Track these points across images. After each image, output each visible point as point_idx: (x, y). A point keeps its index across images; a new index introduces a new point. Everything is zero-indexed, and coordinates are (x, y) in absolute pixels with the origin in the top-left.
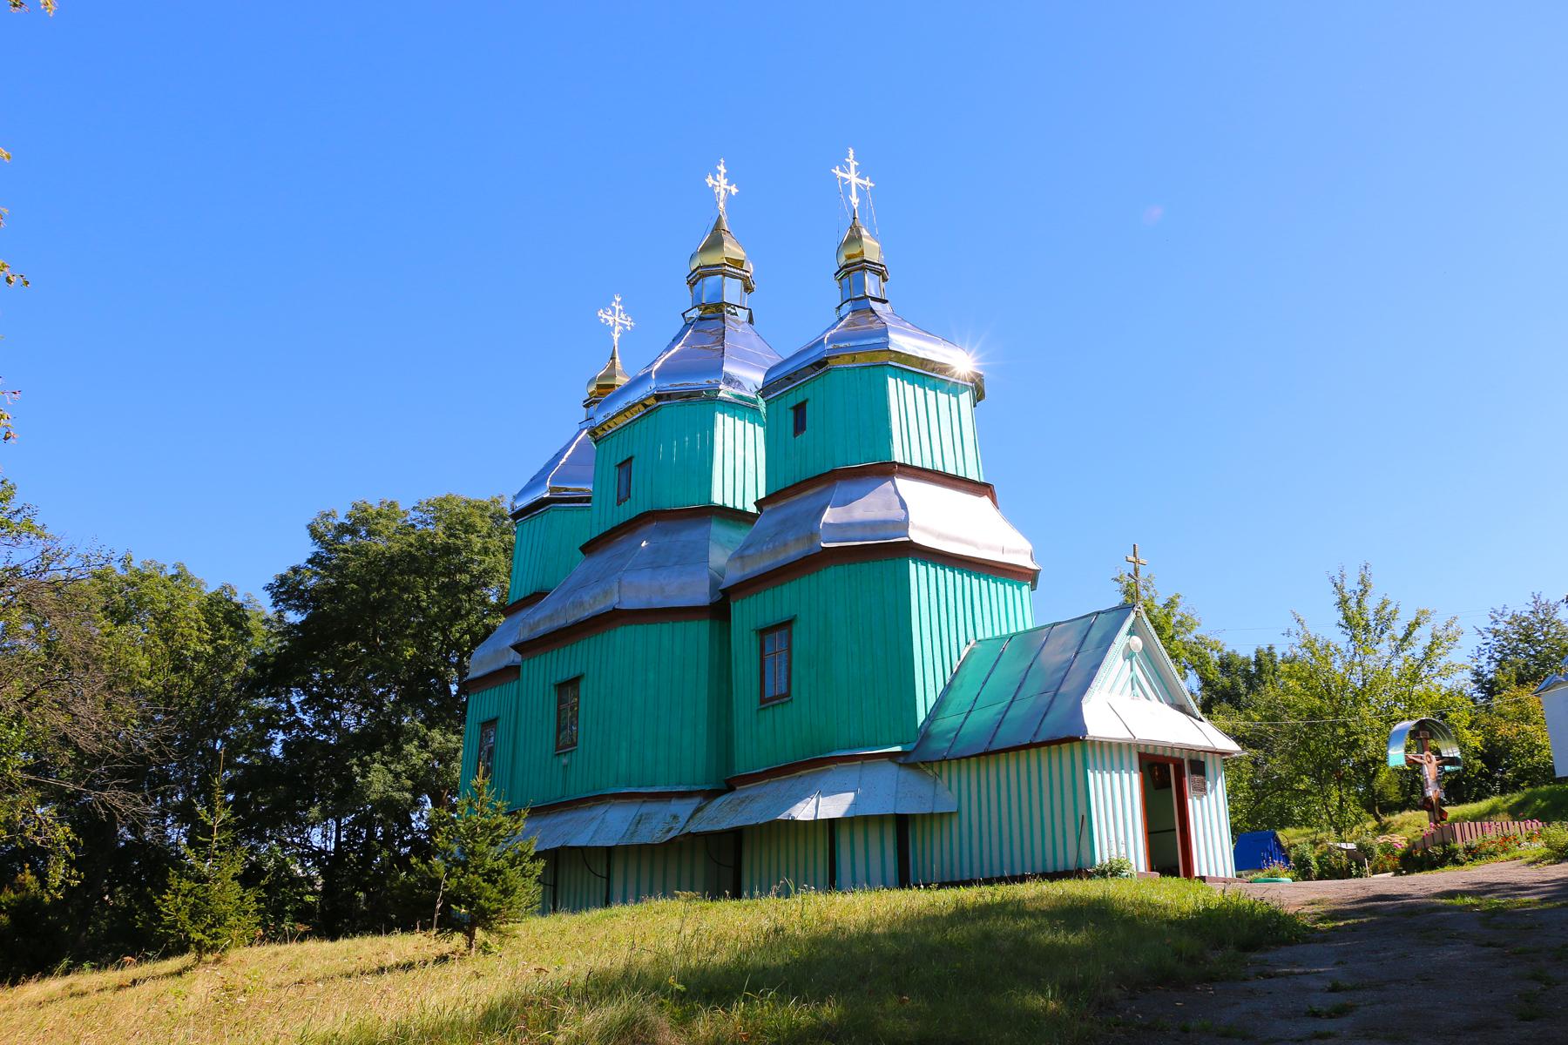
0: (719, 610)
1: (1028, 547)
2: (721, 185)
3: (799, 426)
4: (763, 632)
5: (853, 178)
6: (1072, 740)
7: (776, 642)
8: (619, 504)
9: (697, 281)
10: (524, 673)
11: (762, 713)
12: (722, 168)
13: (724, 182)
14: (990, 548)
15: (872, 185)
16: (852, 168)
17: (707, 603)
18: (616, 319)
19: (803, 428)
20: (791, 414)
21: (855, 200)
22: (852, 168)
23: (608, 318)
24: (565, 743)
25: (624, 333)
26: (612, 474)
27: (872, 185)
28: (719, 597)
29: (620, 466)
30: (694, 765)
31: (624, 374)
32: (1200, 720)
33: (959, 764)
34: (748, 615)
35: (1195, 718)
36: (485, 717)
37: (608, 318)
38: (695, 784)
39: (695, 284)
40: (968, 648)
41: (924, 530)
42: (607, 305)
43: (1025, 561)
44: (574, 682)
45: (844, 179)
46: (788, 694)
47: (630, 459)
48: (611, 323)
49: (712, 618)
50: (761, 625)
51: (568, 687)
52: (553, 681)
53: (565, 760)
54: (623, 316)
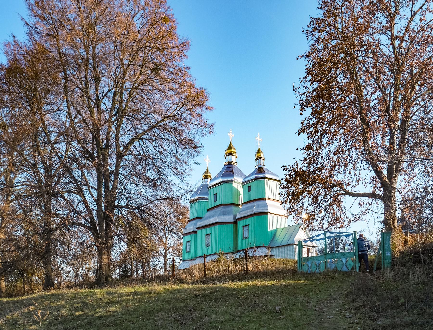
0: (235, 223)
2: (231, 135)
3: (249, 190)
4: (243, 226)
5: (259, 139)
6: (292, 244)
7: (245, 228)
8: (214, 202)
12: (231, 131)
13: (231, 136)
19: (250, 191)
20: (248, 188)
30: (231, 250)
34: (241, 224)
44: (250, 186)
46: (248, 237)
47: (216, 194)
49: (234, 224)
50: (243, 225)
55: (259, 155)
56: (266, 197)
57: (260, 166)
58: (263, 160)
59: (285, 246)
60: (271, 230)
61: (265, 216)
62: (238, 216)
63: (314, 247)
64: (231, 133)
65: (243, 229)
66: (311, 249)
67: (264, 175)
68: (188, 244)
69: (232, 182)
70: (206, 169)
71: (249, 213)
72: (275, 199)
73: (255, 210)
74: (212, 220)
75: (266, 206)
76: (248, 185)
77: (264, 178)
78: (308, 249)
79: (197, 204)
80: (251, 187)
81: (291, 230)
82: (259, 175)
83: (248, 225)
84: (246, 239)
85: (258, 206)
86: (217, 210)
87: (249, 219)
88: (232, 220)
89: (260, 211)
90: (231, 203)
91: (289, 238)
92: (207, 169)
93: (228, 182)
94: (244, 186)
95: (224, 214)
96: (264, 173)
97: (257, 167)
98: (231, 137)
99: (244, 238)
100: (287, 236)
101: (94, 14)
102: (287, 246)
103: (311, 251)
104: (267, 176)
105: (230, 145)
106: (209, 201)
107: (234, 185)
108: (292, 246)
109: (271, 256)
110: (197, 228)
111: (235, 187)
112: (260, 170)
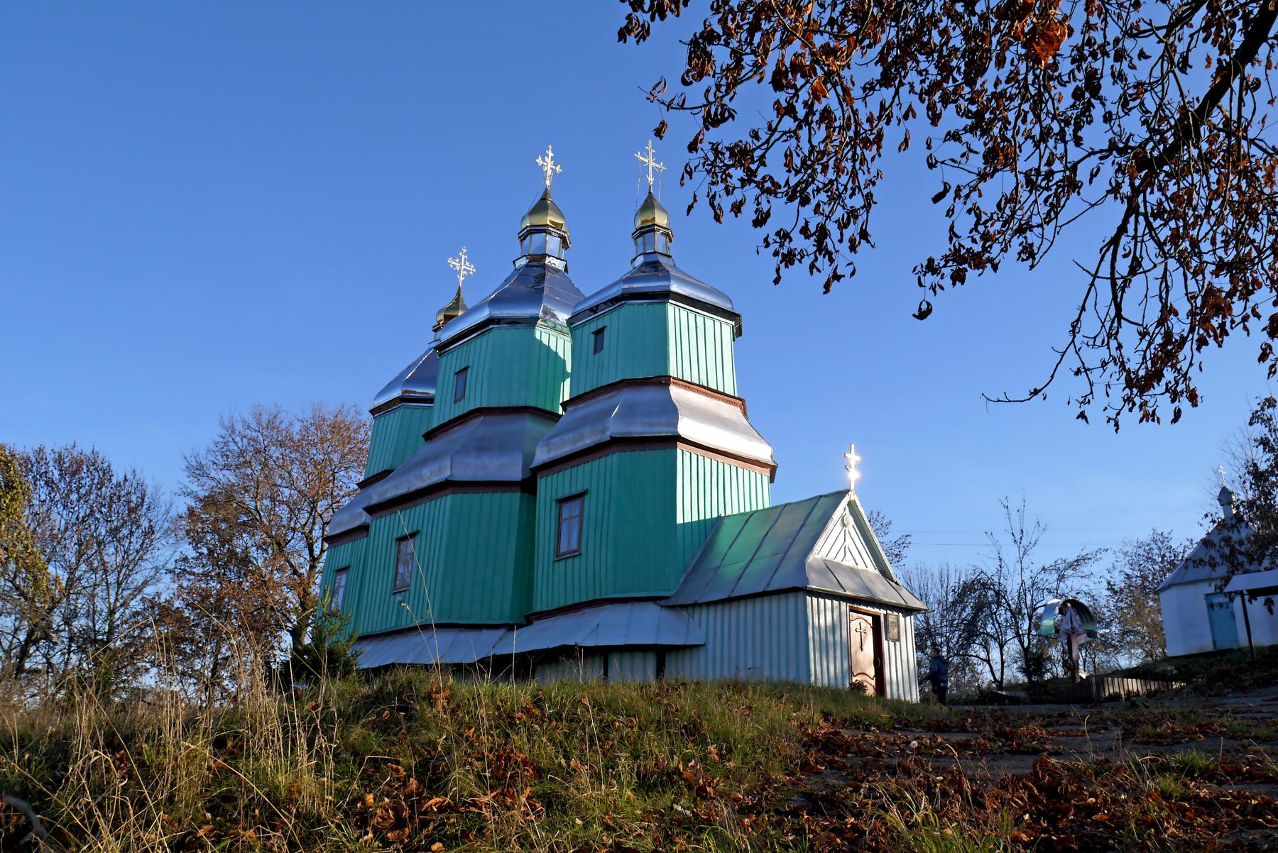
0: (528, 486)
2: (548, 164)
3: (598, 348)
4: (562, 501)
6: (795, 590)
8: (455, 402)
10: (372, 530)
11: (557, 564)
16: (650, 154)
18: (463, 267)
19: (602, 348)
20: (592, 337)
22: (650, 154)
25: (467, 277)
34: (549, 487)
47: (466, 369)
52: (395, 536)
55: (648, 216)
56: (673, 372)
57: (651, 258)
58: (663, 238)
59: (758, 601)
60: (688, 520)
61: (653, 456)
62: (541, 456)
63: (908, 611)
64: (548, 160)
66: (891, 619)
67: (665, 283)
68: (343, 579)
69: (532, 322)
70: (454, 295)
71: (588, 441)
72: (713, 386)
73: (615, 428)
74: (429, 476)
75: (671, 411)
76: (594, 327)
77: (666, 295)
78: (876, 618)
79: (393, 419)
80: (606, 332)
81: (786, 525)
82: (635, 286)
83: (582, 495)
84: (569, 561)
85: (630, 412)
86: (461, 434)
88: (516, 474)
89: (638, 429)
90: (522, 404)
91: (778, 557)
92: (459, 294)
93: (514, 322)
94: (578, 332)
95: (482, 447)
96: (667, 277)
97: (640, 260)
98: (549, 172)
99: (560, 557)
100: (767, 550)
102: (766, 599)
103: (893, 631)
104: (675, 288)
105: (544, 199)
107: (542, 334)
108: (791, 597)
110: (371, 510)
111: (553, 348)
112: (653, 266)
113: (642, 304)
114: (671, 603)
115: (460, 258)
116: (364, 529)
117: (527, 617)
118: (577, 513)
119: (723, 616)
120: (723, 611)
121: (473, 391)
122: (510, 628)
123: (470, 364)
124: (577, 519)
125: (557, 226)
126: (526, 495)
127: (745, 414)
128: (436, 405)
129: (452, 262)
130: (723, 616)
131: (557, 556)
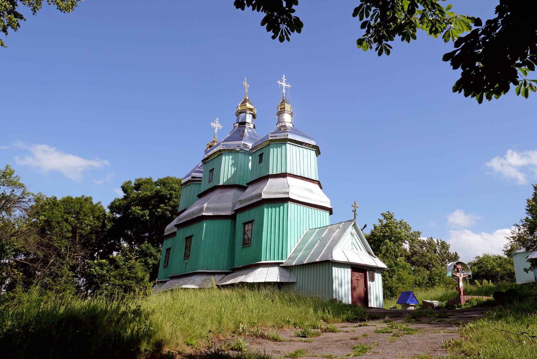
0: (233, 217)
1: (328, 200)
3: (261, 161)
4: (245, 224)
5: (284, 84)
8: (209, 183)
9: (239, 114)
10: (177, 234)
11: (243, 249)
14: (316, 200)
15: (290, 86)
16: (284, 81)
17: (230, 214)
18: (216, 125)
19: (262, 162)
20: (259, 157)
21: (284, 91)
22: (284, 81)
23: (214, 125)
24: (187, 256)
25: (219, 130)
26: (208, 173)
27: (290, 86)
28: (234, 212)
29: (210, 171)
30: (223, 266)
31: (251, 139)
32: (375, 257)
33: (303, 266)
34: (241, 218)
35: (373, 256)
36: (168, 247)
37: (214, 125)
38: (223, 270)
39: (238, 116)
40: (306, 231)
41: (294, 194)
42: (214, 121)
43: (328, 205)
44: (191, 237)
45: (281, 85)
47: (213, 169)
48: (215, 126)
51: (189, 239)
52: (185, 237)
53: (186, 261)
54: (219, 124)
65: (244, 229)
76: (259, 153)
80: (264, 155)
87: (255, 209)
90: (233, 184)
101: (392, 247)
106: (202, 184)
109: (275, 340)
113: (277, 144)
114: (284, 265)
115: (216, 122)
116: (174, 234)
117: (232, 270)
118: (251, 228)
119: (322, 271)
120: (329, 266)
121: (215, 179)
122: (227, 274)
123: (215, 168)
124: (251, 231)
125: (251, 110)
126: (234, 220)
127: (321, 188)
128: (203, 183)
129: (213, 124)
130: (322, 271)
131: (243, 245)
